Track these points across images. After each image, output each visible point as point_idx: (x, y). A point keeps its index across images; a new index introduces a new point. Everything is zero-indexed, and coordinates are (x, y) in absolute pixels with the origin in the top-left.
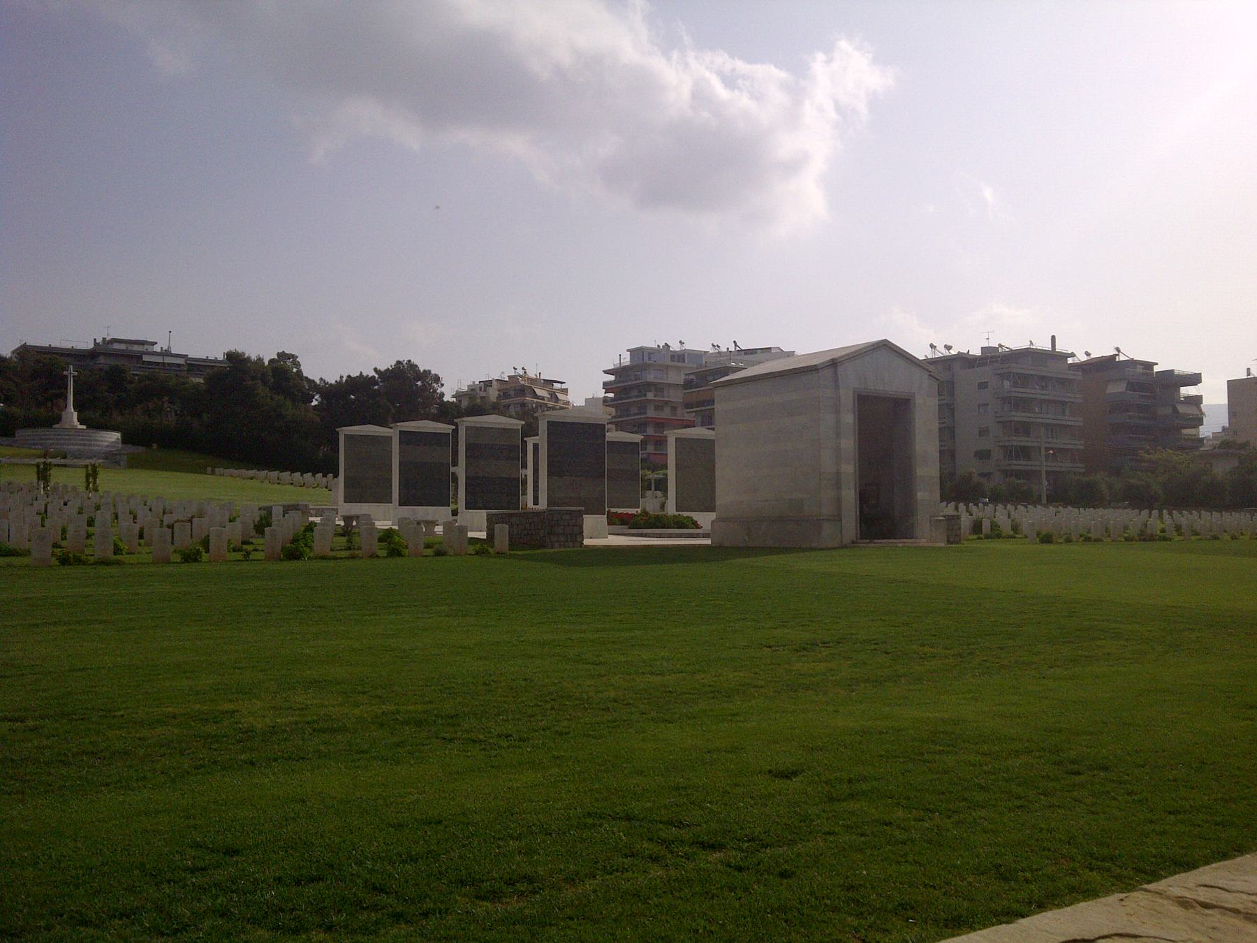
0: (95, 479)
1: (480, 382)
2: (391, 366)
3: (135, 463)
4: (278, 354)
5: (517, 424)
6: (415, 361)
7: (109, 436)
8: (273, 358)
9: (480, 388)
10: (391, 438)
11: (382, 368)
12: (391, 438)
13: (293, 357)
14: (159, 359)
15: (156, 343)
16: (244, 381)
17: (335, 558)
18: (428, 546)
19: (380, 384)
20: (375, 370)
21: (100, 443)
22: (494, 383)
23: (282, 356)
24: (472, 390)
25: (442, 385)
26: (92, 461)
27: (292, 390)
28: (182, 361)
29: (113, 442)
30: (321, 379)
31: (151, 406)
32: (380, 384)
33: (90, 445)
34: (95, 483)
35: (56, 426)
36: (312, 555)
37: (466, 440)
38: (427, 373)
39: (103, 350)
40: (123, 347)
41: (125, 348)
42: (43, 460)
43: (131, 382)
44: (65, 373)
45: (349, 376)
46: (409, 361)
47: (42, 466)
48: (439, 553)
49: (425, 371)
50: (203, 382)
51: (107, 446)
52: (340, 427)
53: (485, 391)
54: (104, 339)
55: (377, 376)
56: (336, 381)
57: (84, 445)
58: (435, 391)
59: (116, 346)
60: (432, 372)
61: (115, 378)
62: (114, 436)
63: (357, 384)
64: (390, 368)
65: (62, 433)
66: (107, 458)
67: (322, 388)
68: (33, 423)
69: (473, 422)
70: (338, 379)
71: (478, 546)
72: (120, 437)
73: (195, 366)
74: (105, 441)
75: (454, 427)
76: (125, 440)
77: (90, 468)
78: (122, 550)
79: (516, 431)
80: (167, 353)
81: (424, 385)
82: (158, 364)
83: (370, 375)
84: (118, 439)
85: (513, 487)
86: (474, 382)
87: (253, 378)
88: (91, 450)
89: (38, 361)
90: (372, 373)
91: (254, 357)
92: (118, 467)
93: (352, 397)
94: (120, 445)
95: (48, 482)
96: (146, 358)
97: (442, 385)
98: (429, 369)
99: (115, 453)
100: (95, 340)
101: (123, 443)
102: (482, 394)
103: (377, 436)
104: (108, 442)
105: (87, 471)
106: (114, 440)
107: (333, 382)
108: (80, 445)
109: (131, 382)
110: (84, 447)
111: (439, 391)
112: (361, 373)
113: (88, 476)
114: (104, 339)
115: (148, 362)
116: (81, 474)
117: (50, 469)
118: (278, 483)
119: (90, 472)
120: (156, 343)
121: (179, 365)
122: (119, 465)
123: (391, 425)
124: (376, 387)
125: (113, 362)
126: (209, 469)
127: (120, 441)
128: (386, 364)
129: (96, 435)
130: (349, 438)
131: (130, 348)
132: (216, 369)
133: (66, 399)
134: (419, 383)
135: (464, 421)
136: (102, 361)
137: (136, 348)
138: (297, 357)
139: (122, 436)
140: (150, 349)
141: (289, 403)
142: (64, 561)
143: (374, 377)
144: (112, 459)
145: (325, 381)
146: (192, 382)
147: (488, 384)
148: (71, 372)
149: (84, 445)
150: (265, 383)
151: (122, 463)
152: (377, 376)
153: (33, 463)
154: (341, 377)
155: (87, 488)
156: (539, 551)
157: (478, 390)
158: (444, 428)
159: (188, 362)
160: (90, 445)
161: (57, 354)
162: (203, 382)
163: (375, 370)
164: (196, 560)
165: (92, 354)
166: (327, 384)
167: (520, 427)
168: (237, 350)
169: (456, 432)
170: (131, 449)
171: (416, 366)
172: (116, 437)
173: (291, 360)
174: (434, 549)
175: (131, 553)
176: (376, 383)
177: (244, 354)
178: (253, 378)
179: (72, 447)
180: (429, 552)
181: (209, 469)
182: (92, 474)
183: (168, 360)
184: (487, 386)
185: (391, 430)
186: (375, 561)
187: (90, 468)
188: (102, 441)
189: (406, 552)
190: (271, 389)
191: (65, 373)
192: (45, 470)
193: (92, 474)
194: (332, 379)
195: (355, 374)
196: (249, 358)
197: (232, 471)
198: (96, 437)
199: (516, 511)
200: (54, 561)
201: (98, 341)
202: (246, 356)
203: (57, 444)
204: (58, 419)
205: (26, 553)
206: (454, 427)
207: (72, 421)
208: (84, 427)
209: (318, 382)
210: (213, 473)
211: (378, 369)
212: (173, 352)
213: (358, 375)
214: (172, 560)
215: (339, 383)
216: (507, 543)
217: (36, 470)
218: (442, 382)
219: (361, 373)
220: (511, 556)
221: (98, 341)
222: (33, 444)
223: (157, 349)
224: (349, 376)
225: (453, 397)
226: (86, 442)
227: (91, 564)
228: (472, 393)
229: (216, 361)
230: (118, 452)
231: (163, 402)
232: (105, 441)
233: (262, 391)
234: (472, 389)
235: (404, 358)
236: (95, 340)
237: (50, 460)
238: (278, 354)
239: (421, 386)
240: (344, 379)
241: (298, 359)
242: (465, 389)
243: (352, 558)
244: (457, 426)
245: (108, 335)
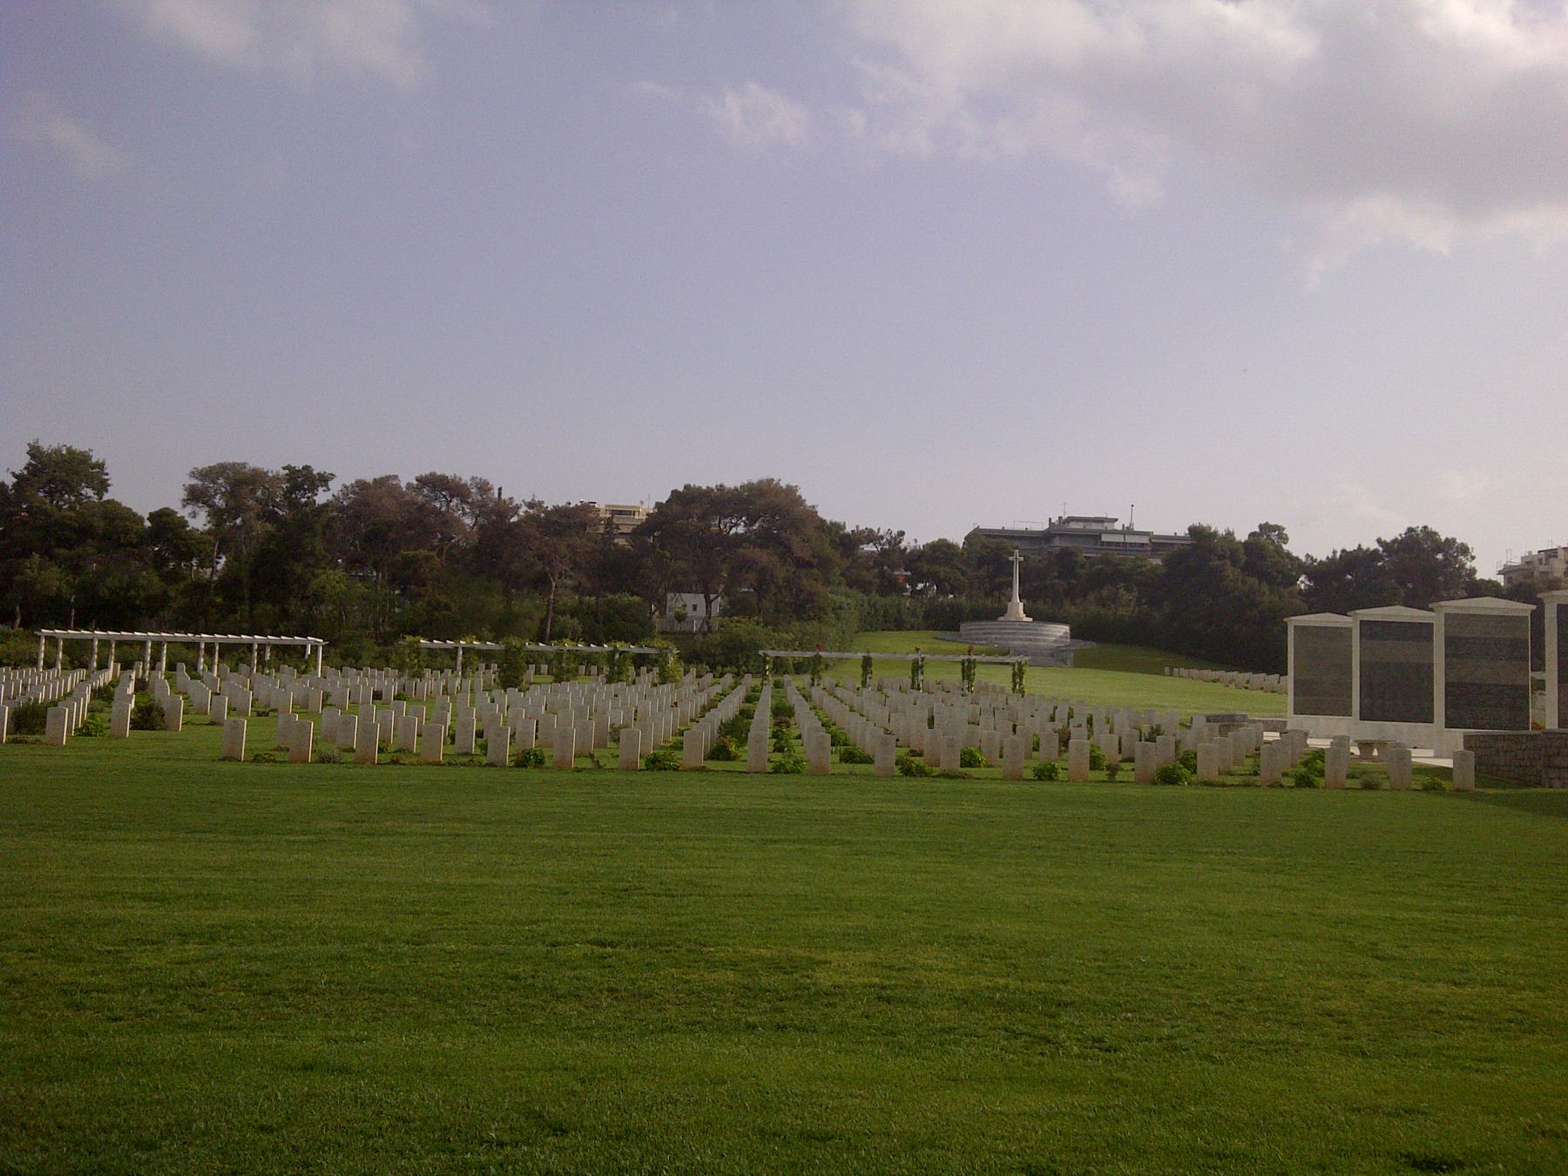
0: (1021, 678)
1: (1539, 552)
2: (1400, 535)
3: (1082, 662)
4: (1261, 527)
5: (1525, 610)
6: (1433, 527)
7: (1055, 630)
8: (1253, 531)
9: (1541, 560)
10: (1350, 630)
11: (1388, 538)
12: (1350, 630)
13: (1279, 529)
14: (1119, 539)
15: (1117, 520)
16: (1210, 561)
17: (1224, 785)
18: (1351, 776)
19: (1387, 559)
20: (1379, 541)
21: (1047, 638)
22: (1561, 553)
23: (1266, 528)
24: (1527, 563)
25: (1473, 558)
26: (1018, 658)
27: (1270, 570)
28: (1145, 540)
29: (1061, 637)
30: (1308, 556)
31: (1105, 593)
32: (1387, 559)
33: (1036, 640)
34: (1020, 684)
35: (1001, 618)
36: (1193, 778)
37: (1446, 632)
38: (1450, 542)
39: (1059, 531)
40: (1079, 526)
41: (1082, 527)
42: (966, 657)
43: (1083, 567)
44: (1011, 558)
45: (1343, 551)
46: (1425, 527)
47: (966, 664)
48: (1369, 786)
49: (1447, 539)
50: (1160, 563)
51: (1055, 641)
52: (1287, 617)
53: (1547, 564)
54: (1060, 518)
55: (1381, 549)
56: (1328, 558)
57: (1030, 640)
58: (1462, 566)
59: (1073, 525)
60: (1457, 540)
61: (1065, 560)
62: (1062, 630)
63: (1354, 561)
64: (1399, 538)
65: (1008, 627)
66: (1052, 656)
67: (1308, 567)
68: (979, 615)
69: (1455, 607)
70: (1330, 555)
71: (1426, 779)
72: (1068, 631)
73: (1159, 545)
74: (1052, 636)
75: (1534, 607)
76: (1074, 635)
77: (1017, 666)
78: (980, 762)
79: (1522, 619)
80: (1128, 531)
81: (1446, 558)
82: (1118, 544)
83: (1372, 548)
84: (1066, 633)
85: (1516, 701)
86: (1530, 553)
87: (1221, 557)
88: (1036, 645)
89: (984, 546)
90: (1374, 546)
91: (1222, 532)
92: (1064, 665)
93: (1349, 577)
94: (1069, 640)
95: (972, 681)
96: (1105, 538)
97: (1473, 558)
98: (1453, 536)
99: (1062, 649)
100: (1050, 519)
101: (1072, 637)
102: (1542, 568)
103: (1337, 628)
104: (1055, 636)
105: (1014, 669)
106: (1061, 634)
107: (1324, 559)
108: (1026, 640)
109: (1083, 567)
110: (1031, 643)
111: (1468, 566)
112: (1360, 545)
113: (1014, 675)
114: (1060, 518)
115: (1107, 542)
116: (1009, 671)
117: (975, 667)
118: (1246, 688)
119: (1017, 671)
120: (1117, 520)
121: (1142, 545)
122: (1066, 664)
123: (1431, 606)
124: (1380, 564)
125: (1066, 544)
126: (1167, 670)
127: (1069, 636)
128: (1394, 530)
129: (1043, 628)
130: (1300, 630)
131: (1088, 527)
132: (1176, 548)
133: (1011, 585)
134: (1440, 556)
135: (1441, 606)
136: (1057, 544)
137: (1095, 526)
138: (1284, 529)
139: (1071, 630)
140: (1109, 526)
141: (1265, 588)
142: (908, 771)
143: (1376, 551)
144: (1056, 657)
145: (1312, 558)
146: (1151, 564)
147: (1551, 554)
148: (1017, 557)
149: (1030, 640)
150: (1234, 562)
151: (1068, 663)
152: (1381, 549)
153: (957, 660)
154: (1335, 552)
155: (1014, 689)
156: (1533, 790)
157: (1537, 562)
158: (1425, 617)
159: (1153, 541)
160: (1036, 640)
161: (1005, 537)
162: (1160, 563)
163: (1379, 541)
164: (1051, 778)
165: (1046, 537)
166: (1314, 560)
167: (1528, 614)
168: (1202, 523)
169: (1538, 616)
170: (1081, 645)
171: (1436, 534)
172: (1064, 631)
173: (1277, 533)
174: (1360, 781)
175: (991, 766)
176: (1380, 558)
177: (1210, 528)
178: (1221, 557)
179: (1015, 642)
180: (1350, 783)
181: (1167, 670)
182: (1018, 675)
183: (1130, 539)
184: (1550, 557)
185: (1432, 614)
186: (1278, 792)
187: (1017, 666)
188: (1048, 635)
189: (1321, 782)
190: (1243, 570)
191: (1011, 558)
192: (969, 668)
193: (1018, 675)
194: (1322, 554)
195: (1351, 547)
196: (1215, 533)
197: (1195, 672)
198: (1042, 631)
199: (1524, 732)
200: (897, 771)
201: (1053, 521)
202: (1212, 530)
203: (1000, 639)
204: (1003, 611)
205: (868, 760)
206: (1534, 607)
207: (1018, 613)
208: (1030, 619)
209: (1304, 559)
210: (1171, 674)
211: (1383, 539)
212: (1135, 530)
213: (1356, 548)
214: (1025, 776)
215: (1331, 561)
216: (1472, 779)
217: (961, 667)
218: (1473, 554)
219: (1360, 545)
220: (1474, 797)
221: (1053, 521)
222: (977, 639)
223: (1118, 526)
224: (1343, 551)
225: (1500, 573)
226: (1031, 637)
227: (934, 777)
228: (1527, 567)
229: (1175, 537)
230: (1065, 649)
231: (1118, 589)
232: (1052, 636)
233: (1232, 573)
234: (1528, 562)
235: (1418, 524)
236: (1050, 519)
237: (974, 657)
238: (1261, 527)
239: (1444, 560)
240: (1338, 555)
241: (1285, 532)
242: (1517, 561)
243: (1245, 786)
244: (1540, 604)
245: (1065, 513)
